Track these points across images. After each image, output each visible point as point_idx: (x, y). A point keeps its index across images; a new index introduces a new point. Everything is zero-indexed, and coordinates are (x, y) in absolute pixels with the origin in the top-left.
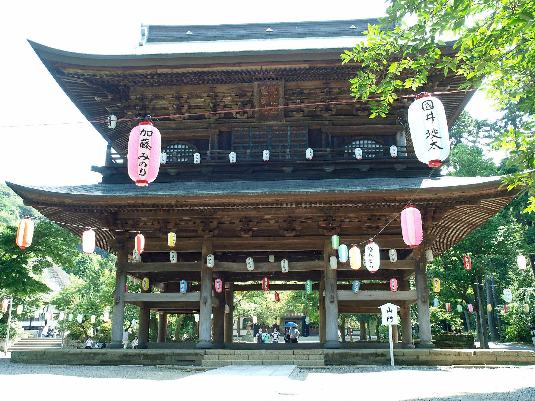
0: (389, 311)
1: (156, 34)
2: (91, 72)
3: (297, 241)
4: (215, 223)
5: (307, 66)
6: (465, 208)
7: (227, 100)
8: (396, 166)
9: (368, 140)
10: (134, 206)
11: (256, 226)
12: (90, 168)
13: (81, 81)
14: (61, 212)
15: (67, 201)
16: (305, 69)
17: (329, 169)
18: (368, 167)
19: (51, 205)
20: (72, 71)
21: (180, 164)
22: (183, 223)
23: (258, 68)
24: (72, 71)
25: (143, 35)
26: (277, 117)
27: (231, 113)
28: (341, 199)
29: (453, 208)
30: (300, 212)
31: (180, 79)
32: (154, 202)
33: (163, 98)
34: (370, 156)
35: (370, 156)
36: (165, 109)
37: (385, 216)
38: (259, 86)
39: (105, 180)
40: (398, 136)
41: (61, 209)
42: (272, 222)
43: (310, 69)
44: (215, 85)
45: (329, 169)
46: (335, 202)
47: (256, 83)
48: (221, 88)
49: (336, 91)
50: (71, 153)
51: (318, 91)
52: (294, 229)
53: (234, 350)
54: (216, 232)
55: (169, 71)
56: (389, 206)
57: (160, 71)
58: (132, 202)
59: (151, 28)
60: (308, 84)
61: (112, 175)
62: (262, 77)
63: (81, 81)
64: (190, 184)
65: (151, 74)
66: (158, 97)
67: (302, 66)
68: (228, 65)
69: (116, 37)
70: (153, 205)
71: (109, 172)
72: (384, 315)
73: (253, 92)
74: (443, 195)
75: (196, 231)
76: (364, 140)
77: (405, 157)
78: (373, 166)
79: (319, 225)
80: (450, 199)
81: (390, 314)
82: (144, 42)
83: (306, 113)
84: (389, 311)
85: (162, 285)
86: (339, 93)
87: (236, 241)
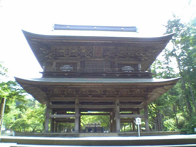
0: (138, 120)
1: (58, 27)
2: (40, 40)
3: (107, 98)
4: (80, 91)
5: (111, 42)
6: (159, 89)
7: (84, 51)
8: (139, 75)
9: (129, 66)
10: (55, 85)
11: (93, 93)
12: (39, 72)
13: (36, 43)
14: (28, 87)
15: (33, 83)
16: (111, 43)
17: (118, 75)
18: (106, 75)
19: (25, 84)
20: (34, 39)
21: (69, 72)
22: (69, 92)
23: (96, 42)
24: (34, 39)
25: (53, 27)
26: (100, 58)
27: (85, 56)
28: (117, 85)
29: (156, 89)
30: (108, 89)
31: (70, 44)
32: (62, 84)
33: (62, 49)
34: (67, 66)
35: (67, 66)
36: (63, 53)
37: (135, 91)
38: (95, 47)
39: (44, 76)
40: (138, 65)
41: (29, 85)
42: (99, 92)
43: (113, 43)
44: (80, 46)
45: (118, 75)
46: (121, 86)
47: (94, 46)
48: (82, 47)
49: (119, 50)
50: (34, 71)
51: (114, 50)
52: (106, 94)
53: (98, 133)
54: (80, 95)
55: (66, 41)
56: (137, 87)
57: (64, 41)
58: (55, 84)
59: (55, 25)
60: (110, 47)
61: (46, 75)
62: (97, 44)
63: (36, 43)
64: (140, 82)
65: (61, 42)
66: (60, 49)
67: (110, 42)
68: (86, 40)
69: (46, 30)
70: (62, 85)
71: (45, 74)
72: (137, 121)
73: (93, 49)
74: (154, 84)
75: (73, 94)
76: (128, 66)
77: (140, 72)
78: (69, 74)
79: (114, 93)
80: (156, 86)
81: (139, 121)
82: (53, 29)
83: (109, 57)
84: (138, 120)
85: (56, 113)
86: (120, 51)
87: (87, 98)
